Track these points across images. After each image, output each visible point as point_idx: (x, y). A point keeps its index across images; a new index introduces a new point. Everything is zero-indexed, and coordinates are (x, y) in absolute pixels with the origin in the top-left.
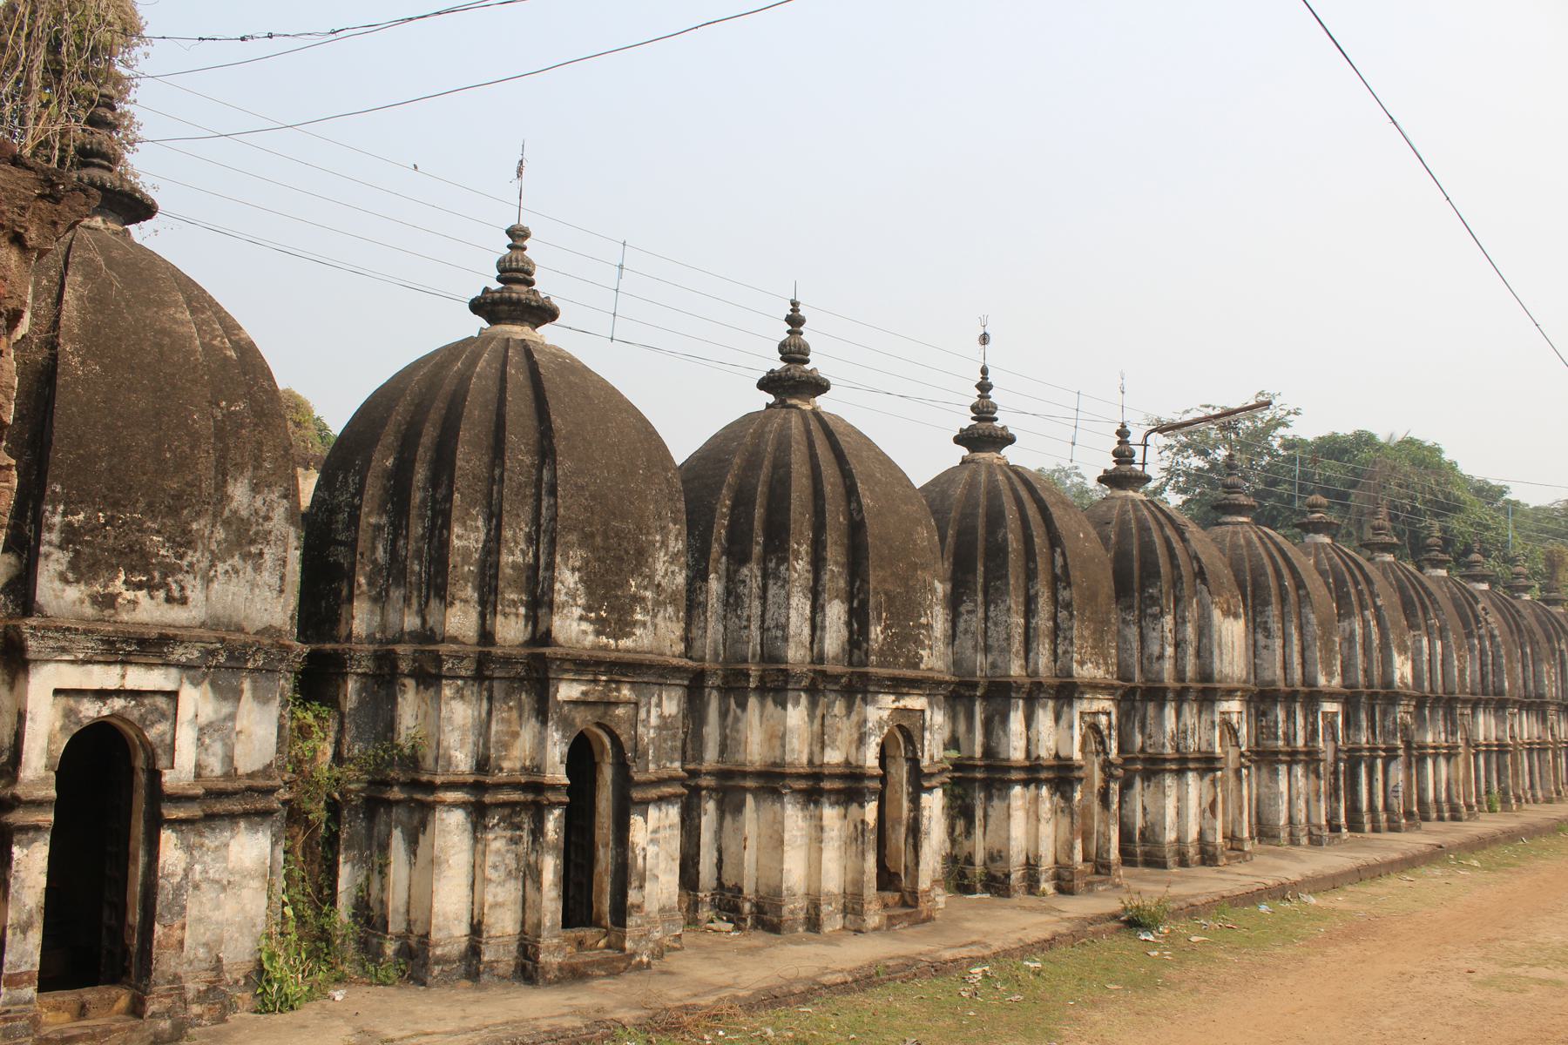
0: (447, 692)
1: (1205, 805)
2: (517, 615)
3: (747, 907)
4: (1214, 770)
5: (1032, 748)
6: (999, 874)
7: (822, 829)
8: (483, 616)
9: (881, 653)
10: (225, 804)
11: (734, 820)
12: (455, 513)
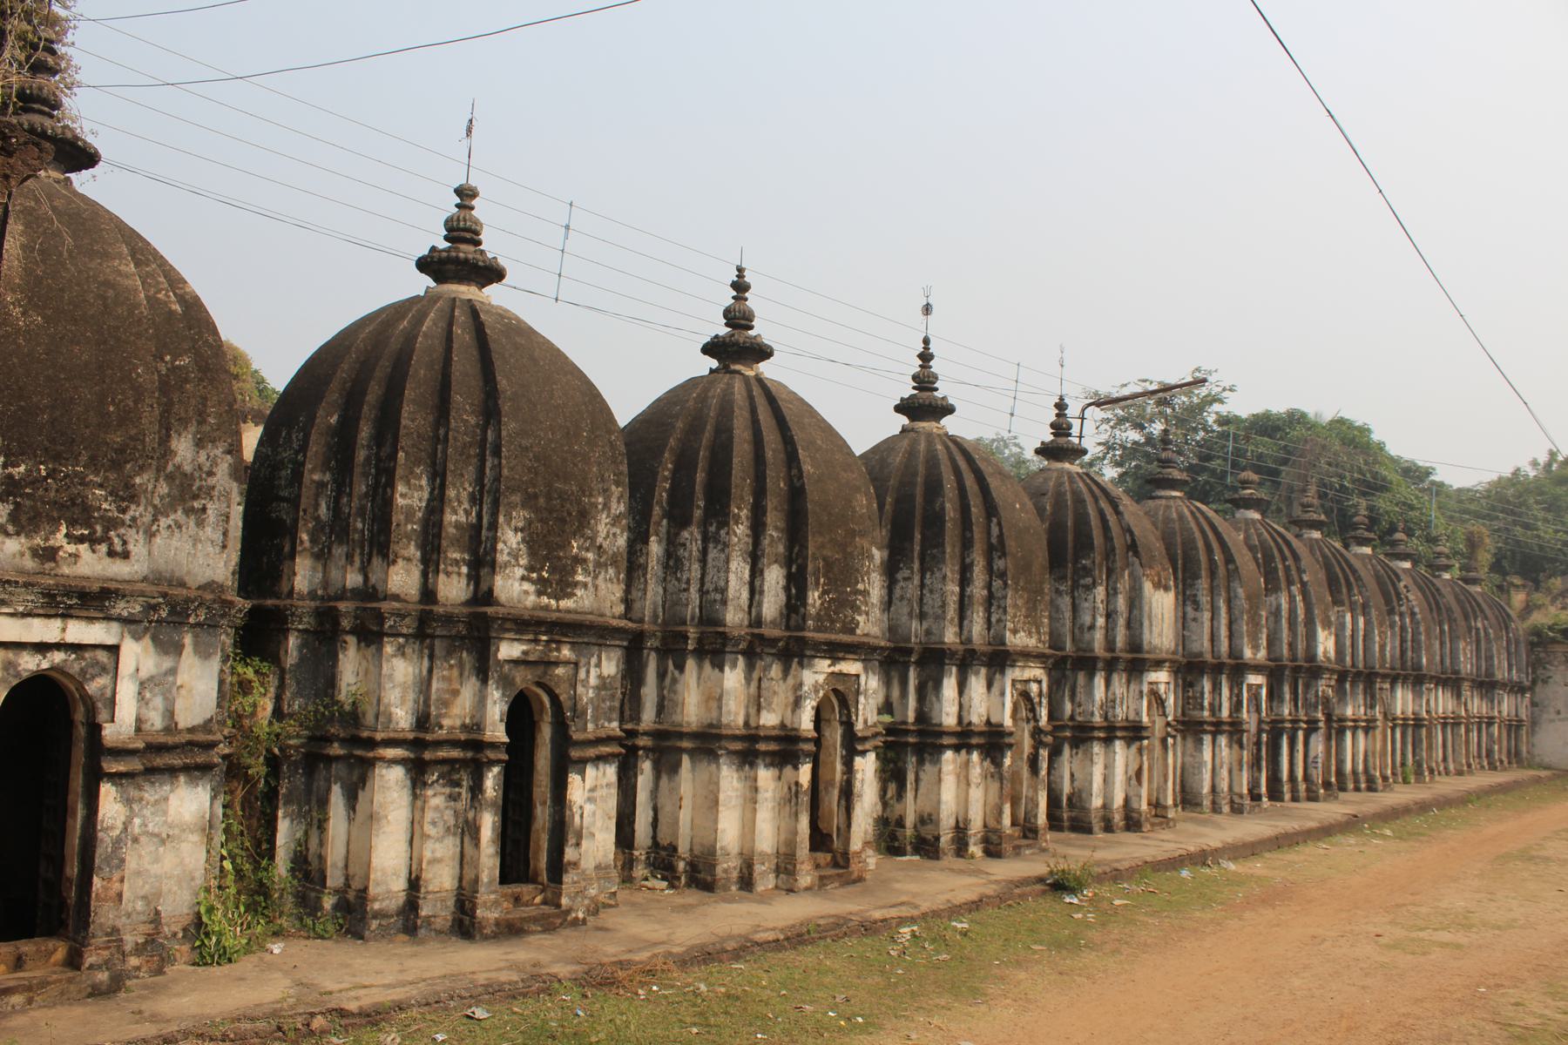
0: (389, 649)
1: (1132, 772)
2: (459, 574)
5: (964, 714)
7: (757, 790)
8: (425, 574)
9: (818, 618)
10: (165, 757)
12: (399, 472)
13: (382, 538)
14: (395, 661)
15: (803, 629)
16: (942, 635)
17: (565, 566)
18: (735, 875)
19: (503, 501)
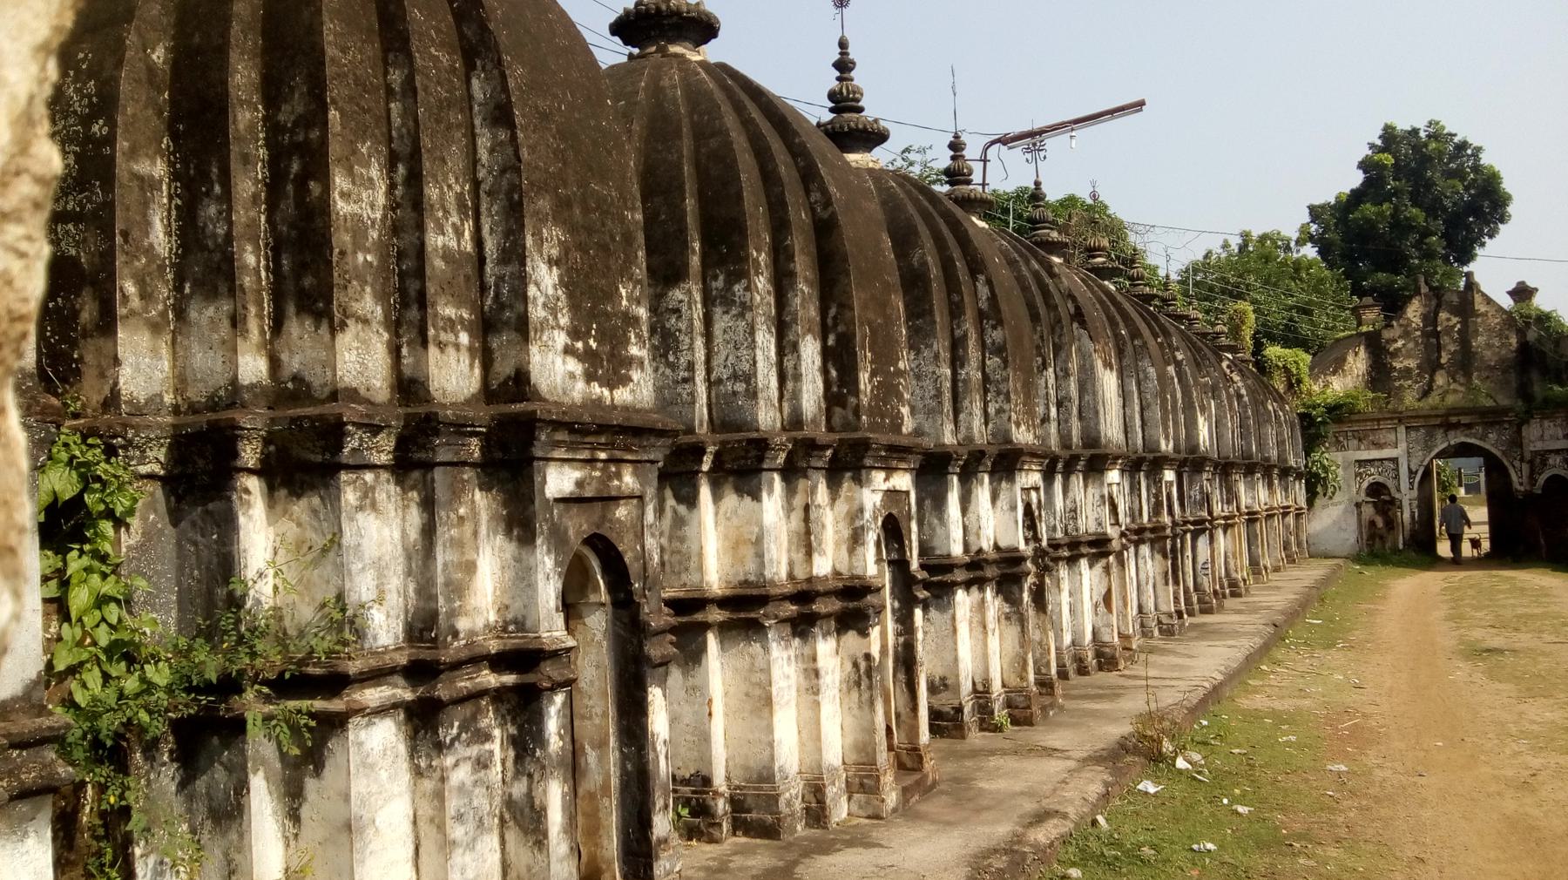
0: (350, 496)
1: (1098, 597)
2: (457, 346)
3: (721, 806)
4: (1106, 555)
5: (972, 539)
6: (947, 709)
7: (817, 673)
8: (395, 351)
9: (872, 412)
11: (685, 674)
12: (335, 149)
13: (308, 281)
14: (360, 516)
15: (856, 429)
16: (939, 433)
17: (616, 328)
18: (798, 805)
19: (528, 208)
